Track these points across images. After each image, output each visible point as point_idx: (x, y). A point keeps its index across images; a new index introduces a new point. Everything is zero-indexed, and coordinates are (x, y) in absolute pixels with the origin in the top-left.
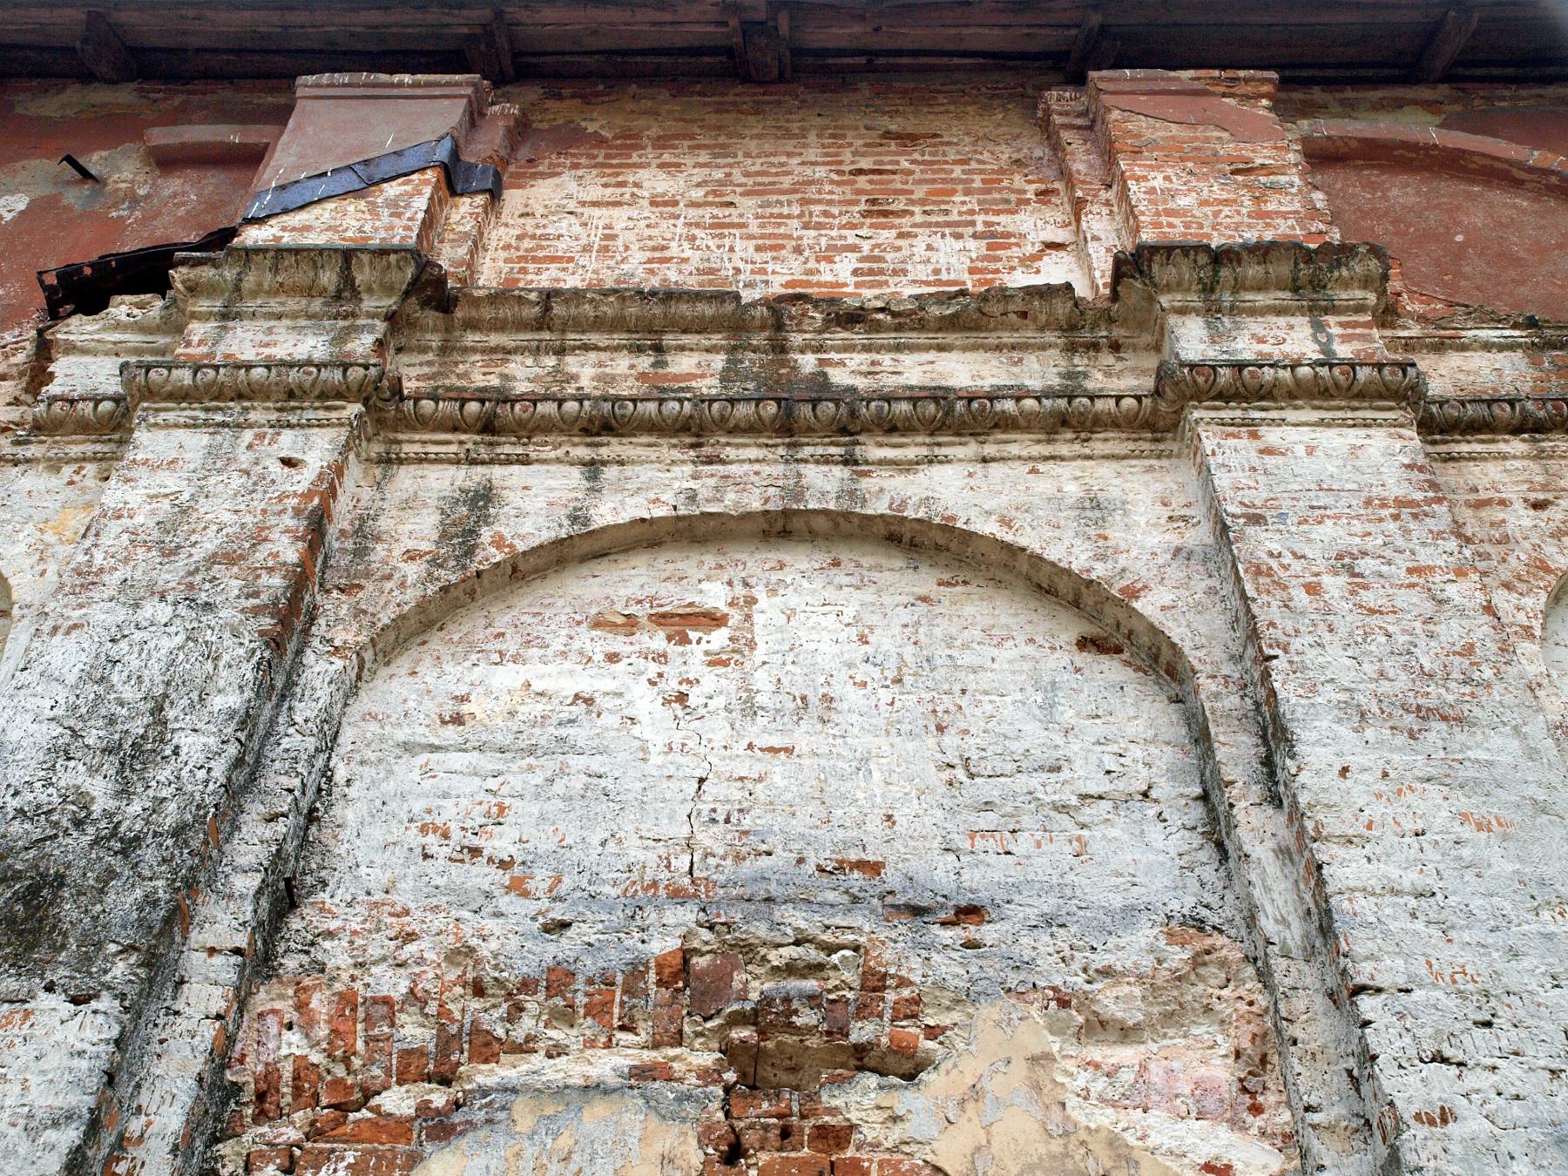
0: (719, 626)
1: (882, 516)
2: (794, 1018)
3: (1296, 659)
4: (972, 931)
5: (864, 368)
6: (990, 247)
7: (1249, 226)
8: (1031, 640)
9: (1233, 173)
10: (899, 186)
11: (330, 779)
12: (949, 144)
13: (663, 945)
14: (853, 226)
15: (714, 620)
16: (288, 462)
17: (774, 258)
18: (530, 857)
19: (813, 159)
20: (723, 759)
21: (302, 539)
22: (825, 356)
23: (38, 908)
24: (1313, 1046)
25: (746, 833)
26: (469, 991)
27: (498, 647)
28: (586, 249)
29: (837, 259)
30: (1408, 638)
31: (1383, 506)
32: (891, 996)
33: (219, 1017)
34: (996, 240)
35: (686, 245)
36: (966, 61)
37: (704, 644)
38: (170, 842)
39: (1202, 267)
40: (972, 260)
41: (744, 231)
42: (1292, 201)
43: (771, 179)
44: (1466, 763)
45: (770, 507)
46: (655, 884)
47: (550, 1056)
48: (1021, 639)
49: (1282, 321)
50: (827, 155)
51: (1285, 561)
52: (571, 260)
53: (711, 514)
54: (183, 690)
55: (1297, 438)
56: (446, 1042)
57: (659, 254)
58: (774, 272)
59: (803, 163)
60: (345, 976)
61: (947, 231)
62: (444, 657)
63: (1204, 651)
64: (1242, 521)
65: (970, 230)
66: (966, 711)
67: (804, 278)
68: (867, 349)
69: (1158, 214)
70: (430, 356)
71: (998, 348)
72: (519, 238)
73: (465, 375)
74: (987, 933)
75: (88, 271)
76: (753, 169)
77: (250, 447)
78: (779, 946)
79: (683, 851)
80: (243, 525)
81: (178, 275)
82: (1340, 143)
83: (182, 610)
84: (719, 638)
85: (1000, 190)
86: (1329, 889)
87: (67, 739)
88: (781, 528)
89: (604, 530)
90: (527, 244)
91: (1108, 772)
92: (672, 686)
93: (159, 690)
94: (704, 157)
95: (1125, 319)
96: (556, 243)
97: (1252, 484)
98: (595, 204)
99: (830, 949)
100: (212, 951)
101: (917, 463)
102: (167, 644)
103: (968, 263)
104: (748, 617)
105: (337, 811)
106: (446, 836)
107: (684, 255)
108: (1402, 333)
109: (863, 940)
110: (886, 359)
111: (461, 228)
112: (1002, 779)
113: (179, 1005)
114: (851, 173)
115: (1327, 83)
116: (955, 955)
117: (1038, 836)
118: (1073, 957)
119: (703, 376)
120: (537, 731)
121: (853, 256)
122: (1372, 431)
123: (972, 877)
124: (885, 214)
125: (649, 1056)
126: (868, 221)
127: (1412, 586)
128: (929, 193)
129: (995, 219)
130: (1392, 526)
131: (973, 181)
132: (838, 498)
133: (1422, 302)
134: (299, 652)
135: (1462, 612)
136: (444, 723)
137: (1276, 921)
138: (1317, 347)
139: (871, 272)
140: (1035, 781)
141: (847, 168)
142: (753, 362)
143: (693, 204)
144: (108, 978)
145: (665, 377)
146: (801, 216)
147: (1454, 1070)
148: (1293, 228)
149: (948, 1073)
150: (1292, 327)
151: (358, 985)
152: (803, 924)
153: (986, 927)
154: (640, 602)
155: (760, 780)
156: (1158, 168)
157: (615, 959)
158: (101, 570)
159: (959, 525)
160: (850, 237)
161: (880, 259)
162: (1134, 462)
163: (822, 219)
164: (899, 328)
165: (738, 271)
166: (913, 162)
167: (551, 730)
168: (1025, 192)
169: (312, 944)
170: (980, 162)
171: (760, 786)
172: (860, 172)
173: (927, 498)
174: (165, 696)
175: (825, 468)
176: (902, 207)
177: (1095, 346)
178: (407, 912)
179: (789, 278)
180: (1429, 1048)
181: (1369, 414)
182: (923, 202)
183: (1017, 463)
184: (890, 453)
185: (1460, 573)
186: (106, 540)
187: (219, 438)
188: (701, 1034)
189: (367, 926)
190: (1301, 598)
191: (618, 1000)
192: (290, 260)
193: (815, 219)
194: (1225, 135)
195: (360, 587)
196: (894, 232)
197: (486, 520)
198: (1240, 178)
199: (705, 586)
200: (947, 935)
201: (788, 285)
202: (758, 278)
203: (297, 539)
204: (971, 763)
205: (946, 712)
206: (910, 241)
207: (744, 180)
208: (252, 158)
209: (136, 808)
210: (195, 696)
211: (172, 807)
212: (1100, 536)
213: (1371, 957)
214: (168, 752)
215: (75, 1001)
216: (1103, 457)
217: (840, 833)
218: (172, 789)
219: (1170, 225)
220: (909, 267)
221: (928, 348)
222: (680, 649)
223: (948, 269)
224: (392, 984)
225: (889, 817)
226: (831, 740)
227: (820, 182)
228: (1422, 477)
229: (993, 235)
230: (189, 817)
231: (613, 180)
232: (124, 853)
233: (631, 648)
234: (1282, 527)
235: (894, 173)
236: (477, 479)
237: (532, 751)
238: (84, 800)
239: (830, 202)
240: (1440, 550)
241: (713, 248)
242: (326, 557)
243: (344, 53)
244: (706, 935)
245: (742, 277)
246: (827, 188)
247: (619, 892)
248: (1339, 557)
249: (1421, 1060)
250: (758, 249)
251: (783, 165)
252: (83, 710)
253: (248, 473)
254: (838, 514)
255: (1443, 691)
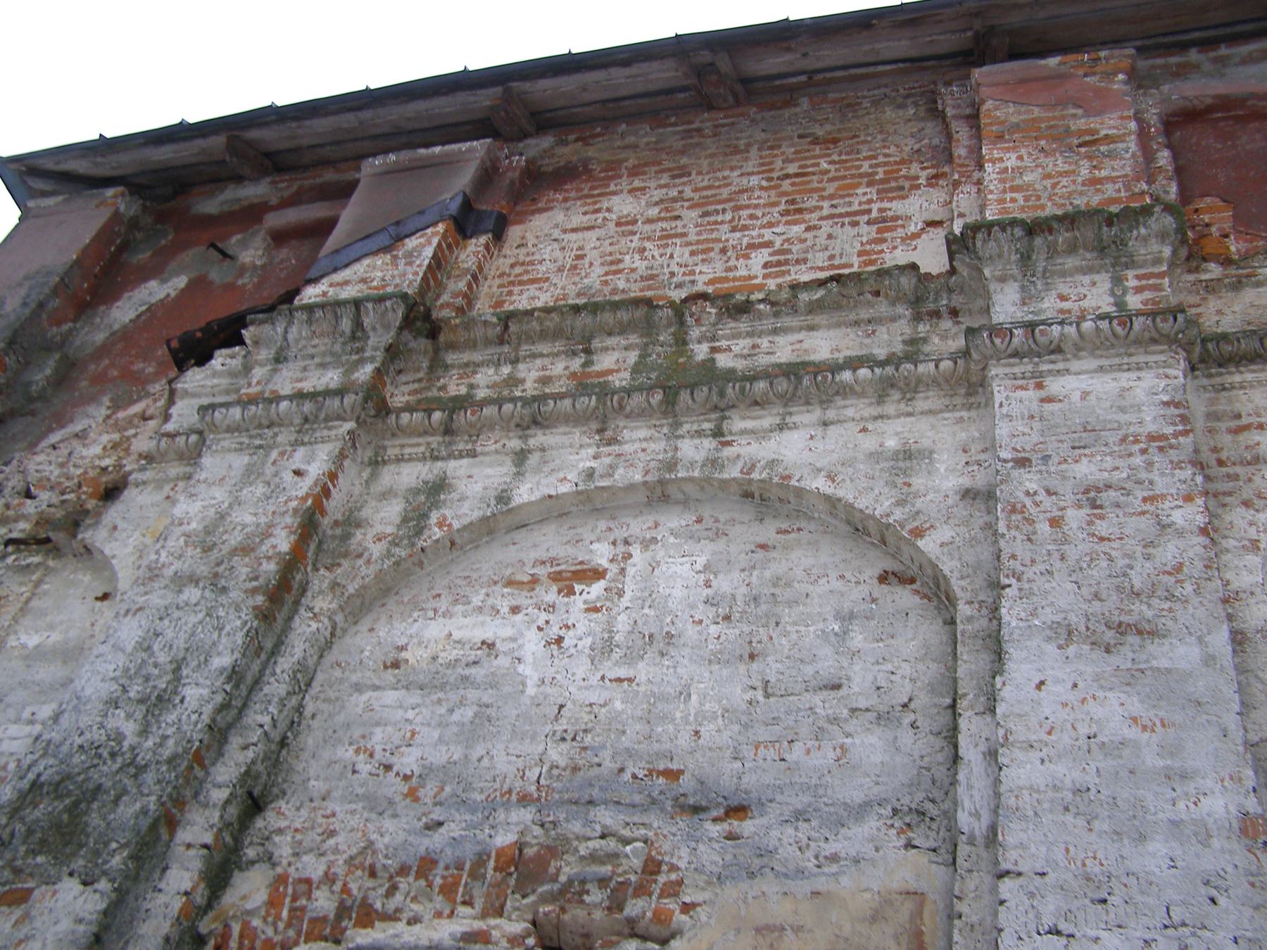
0: (598, 579)
1: (734, 479)
2: (585, 897)
3: (1026, 586)
4: (734, 824)
5: (746, 351)
6: (879, 231)
7: (1081, 194)
8: (842, 577)
9: (1080, 146)
10: (815, 185)
11: (301, 714)
12: (865, 142)
13: (504, 839)
14: (770, 225)
15: (598, 574)
16: (298, 473)
17: (703, 261)
18: (426, 771)
19: (750, 170)
20: (580, 688)
21: (294, 533)
22: (717, 344)
23: (77, 816)
24: (974, 919)
25: (585, 749)
26: (367, 873)
27: (434, 605)
28: (560, 270)
29: (753, 255)
30: (1127, 561)
31: (1136, 441)
32: (662, 879)
33: (186, 893)
34: (885, 223)
35: (637, 256)
36: (888, 67)
37: (585, 595)
38: (164, 768)
39: (1019, 239)
40: (862, 244)
41: (685, 239)
42: (1123, 167)
43: (713, 192)
44: (1148, 673)
45: (649, 478)
46: (510, 792)
47: (409, 923)
48: (833, 575)
49: (1086, 279)
50: (762, 165)
51: (1038, 499)
52: (547, 279)
53: (603, 488)
54: (196, 654)
55: (1077, 385)
56: (343, 911)
57: (614, 265)
58: (700, 272)
59: (742, 175)
60: (285, 862)
61: (847, 220)
62: (395, 616)
63: (968, 580)
64: (1011, 464)
65: (866, 218)
66: (775, 641)
67: (724, 274)
68: (750, 335)
69: (1004, 191)
70: (421, 375)
71: (857, 323)
72: (512, 266)
73: (443, 388)
74: (747, 827)
75: (199, 334)
76: (702, 185)
77: (274, 463)
78: (589, 839)
79: (536, 765)
80: (258, 525)
81: (247, 334)
82: (1196, 102)
83: (208, 594)
84: (597, 588)
85: (896, 179)
86: (1003, 789)
87: (119, 693)
88: (659, 494)
89: (520, 507)
90: (518, 270)
91: (878, 688)
92: (555, 631)
93: (181, 655)
94: (665, 179)
95: (962, 289)
96: (539, 267)
97: (1027, 430)
98: (574, 230)
99: (627, 842)
100: (189, 846)
101: (771, 431)
102: (194, 619)
103: (858, 247)
104: (623, 571)
105: (301, 738)
106: (371, 756)
107: (634, 266)
108: (1204, 277)
109: (651, 834)
110: (764, 343)
111: (465, 265)
112: (791, 698)
113: (162, 885)
114: (778, 178)
115: (1206, 44)
116: (716, 846)
117: (810, 744)
118: (808, 846)
119: (618, 371)
120: (449, 672)
121: (766, 251)
122: (1142, 374)
123: (749, 781)
124: (800, 211)
125: (478, 925)
126: (785, 219)
127: (1143, 513)
128: (839, 189)
129: (887, 205)
130: (1138, 460)
131: (877, 173)
132: (703, 466)
133: (1246, 241)
134: (290, 619)
135: (1180, 533)
136: (386, 667)
137: (970, 814)
138: (1112, 300)
139: (779, 264)
140: (817, 699)
141: (775, 175)
142: (659, 355)
143: (649, 221)
144: (107, 867)
145: (589, 375)
146: (731, 221)
147: (1064, 940)
148: (1119, 191)
149: (689, 940)
150: (1094, 284)
151: (292, 870)
152: (608, 822)
153: (748, 823)
154: (544, 563)
155: (605, 705)
156: (1014, 149)
157: (468, 852)
158: (163, 566)
159: (793, 483)
160: (767, 234)
161: (789, 251)
162: (946, 415)
163: (749, 222)
164: (776, 315)
165: (672, 274)
166: (830, 163)
167: (460, 670)
168: (917, 178)
169: (268, 839)
170: (886, 155)
171: (603, 710)
172: (787, 176)
173: (773, 461)
174: (184, 659)
175: (697, 441)
176: (814, 203)
177: (936, 314)
178: (334, 815)
179: (711, 276)
180: (1048, 921)
181: (1142, 358)
182: (831, 197)
183: (851, 424)
184: (749, 424)
185: (1188, 498)
186: (170, 543)
187: (255, 457)
188: (518, 909)
189: (306, 825)
190: (1044, 528)
191: (463, 882)
192: (319, 313)
193: (742, 222)
194: (1080, 112)
195: (339, 565)
196: (803, 227)
197: (436, 505)
198: (1083, 150)
199: (595, 546)
200: (715, 830)
201: (711, 282)
202: (687, 278)
203: (291, 532)
204: (770, 685)
205: (760, 642)
206: (814, 233)
207: (692, 195)
208: (324, 228)
209: (150, 743)
210: (202, 658)
211: (171, 742)
212: (905, 484)
213: (1021, 845)
214: (177, 701)
215: (85, 884)
216: (922, 413)
217: (656, 746)
218: (174, 729)
219: (1013, 200)
220: (810, 256)
221: (800, 329)
222: (566, 599)
223: (841, 255)
224: (313, 867)
225: (697, 733)
226: (665, 670)
227: (751, 189)
228: (1177, 412)
229: (884, 220)
230: (180, 750)
231: (591, 208)
232: (135, 776)
233: (530, 601)
234: (1044, 468)
235: (814, 174)
236: (435, 472)
237: (442, 687)
238: (119, 737)
239: (756, 206)
240: (1176, 479)
241: (657, 257)
242: (320, 542)
243: (410, 132)
244: (537, 831)
245: (675, 280)
246: (757, 193)
247: (484, 797)
248: (1087, 491)
249: (1039, 934)
250: (692, 253)
251: (725, 178)
252: (132, 672)
253: (269, 484)
254: (701, 480)
255: (1144, 608)
